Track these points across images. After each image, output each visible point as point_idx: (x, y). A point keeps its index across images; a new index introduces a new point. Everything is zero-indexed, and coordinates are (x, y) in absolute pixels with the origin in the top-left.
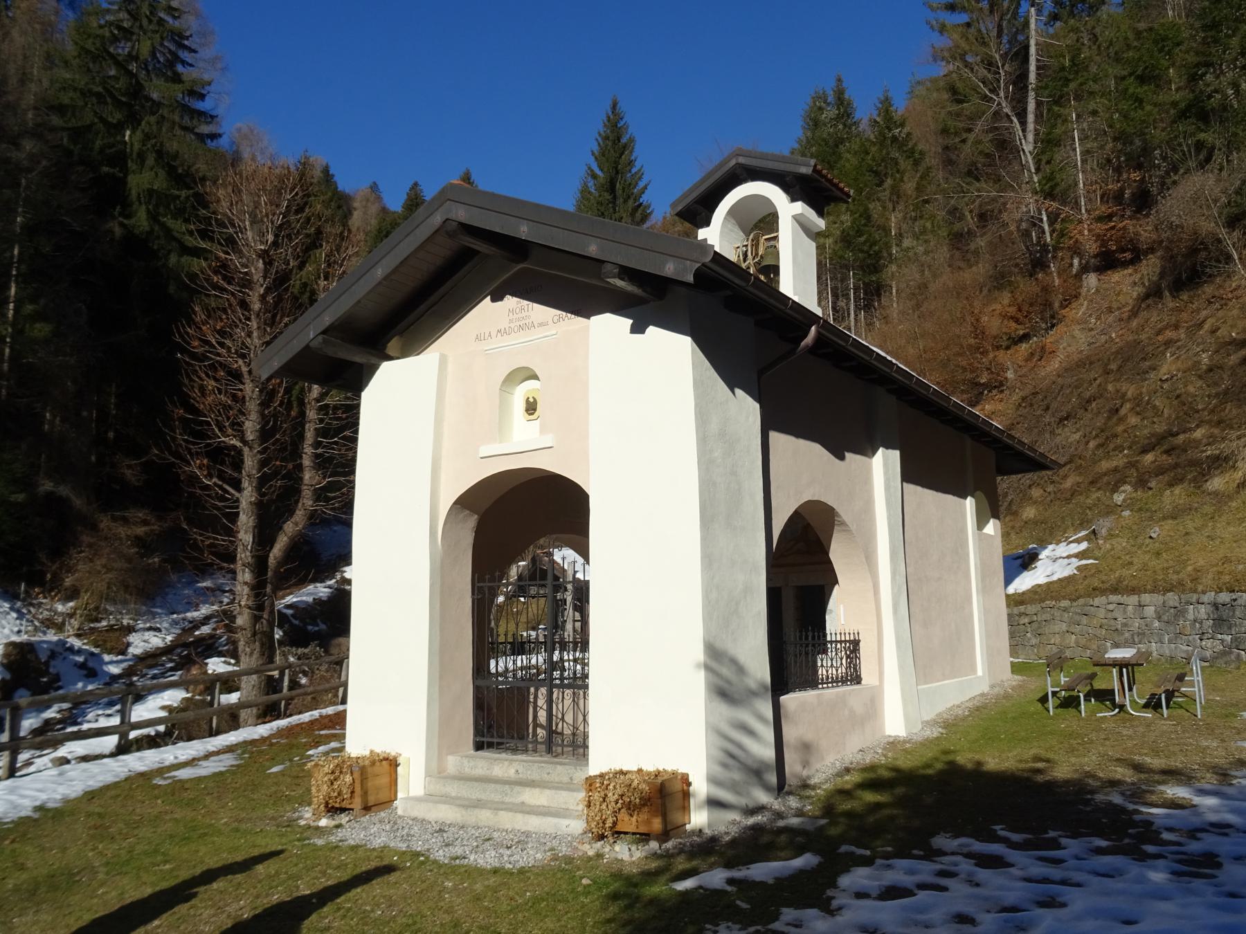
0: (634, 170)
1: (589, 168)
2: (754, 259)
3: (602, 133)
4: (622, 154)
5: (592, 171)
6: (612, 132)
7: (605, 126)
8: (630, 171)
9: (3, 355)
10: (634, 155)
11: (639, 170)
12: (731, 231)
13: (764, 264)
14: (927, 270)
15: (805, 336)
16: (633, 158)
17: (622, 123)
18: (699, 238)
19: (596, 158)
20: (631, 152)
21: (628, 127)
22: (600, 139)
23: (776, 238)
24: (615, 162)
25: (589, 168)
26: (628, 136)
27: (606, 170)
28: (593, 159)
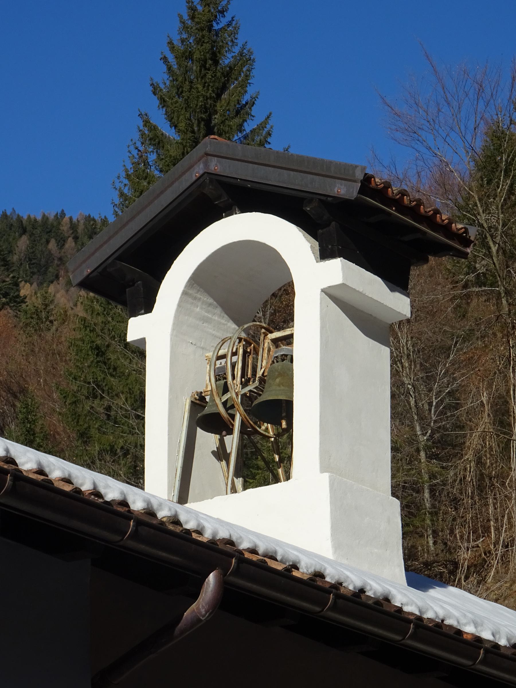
0: (249, 126)
1: (147, 123)
2: (244, 384)
3: (177, 43)
4: (224, 88)
5: (153, 128)
6: (199, 42)
7: (185, 27)
8: (240, 128)
9: (130, 525)
10: (251, 91)
11: (262, 126)
12: (205, 320)
13: (266, 397)
14: (98, 466)
15: (195, 596)
16: (247, 98)
17: (223, 22)
18: (130, 338)
19: (163, 101)
20: (244, 85)
21: (237, 28)
22: (171, 58)
23: (289, 340)
24: (205, 109)
25: (147, 123)
26: (236, 50)
27: (182, 125)
28: (155, 101)
